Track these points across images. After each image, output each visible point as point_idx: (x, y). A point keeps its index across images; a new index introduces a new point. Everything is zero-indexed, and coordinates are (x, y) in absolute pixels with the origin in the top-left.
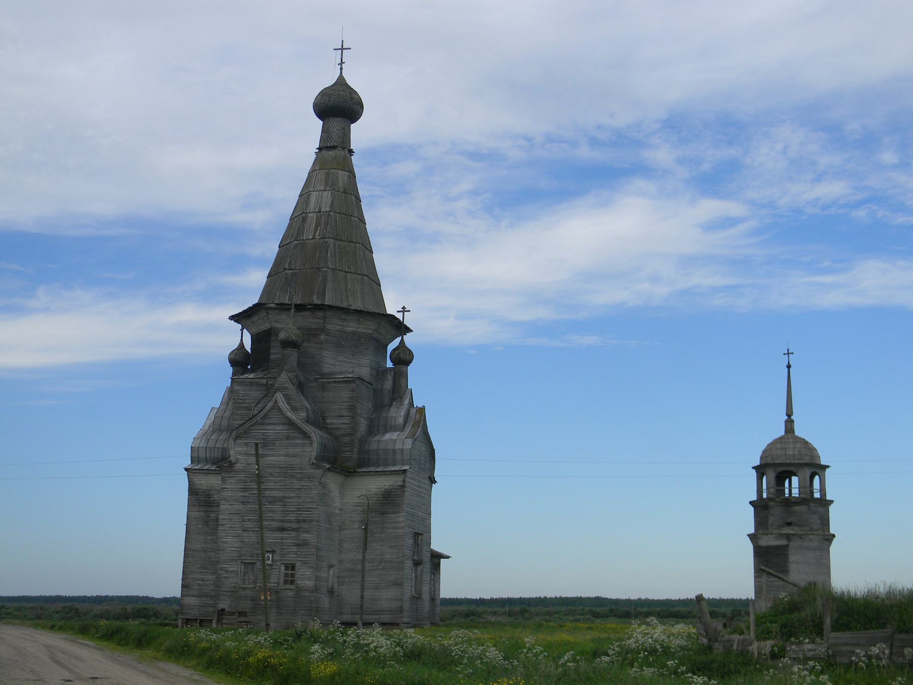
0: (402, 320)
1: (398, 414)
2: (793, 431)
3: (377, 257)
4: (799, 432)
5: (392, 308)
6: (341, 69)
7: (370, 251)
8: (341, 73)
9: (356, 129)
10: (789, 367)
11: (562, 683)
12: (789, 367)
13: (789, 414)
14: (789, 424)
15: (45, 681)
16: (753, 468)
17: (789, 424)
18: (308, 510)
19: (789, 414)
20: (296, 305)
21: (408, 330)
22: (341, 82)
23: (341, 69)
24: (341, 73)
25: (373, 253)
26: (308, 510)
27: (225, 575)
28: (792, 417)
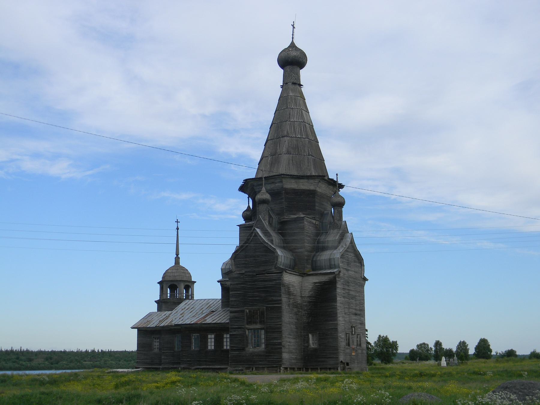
0: (336, 180)
1: (332, 237)
2: (179, 263)
3: (321, 145)
4: (181, 264)
5: (332, 176)
6: (293, 38)
7: (317, 142)
8: (293, 40)
9: (303, 72)
10: (178, 229)
11: (59, 394)
12: (178, 229)
13: (177, 255)
14: (177, 259)
15: (502, 388)
16: (218, 282)
17: (177, 259)
18: (240, 296)
19: (177, 255)
20: (265, 178)
21: (341, 186)
22: (292, 45)
23: (293, 38)
24: (293, 40)
25: (318, 143)
26: (240, 296)
27: (359, 326)
28: (179, 256)
